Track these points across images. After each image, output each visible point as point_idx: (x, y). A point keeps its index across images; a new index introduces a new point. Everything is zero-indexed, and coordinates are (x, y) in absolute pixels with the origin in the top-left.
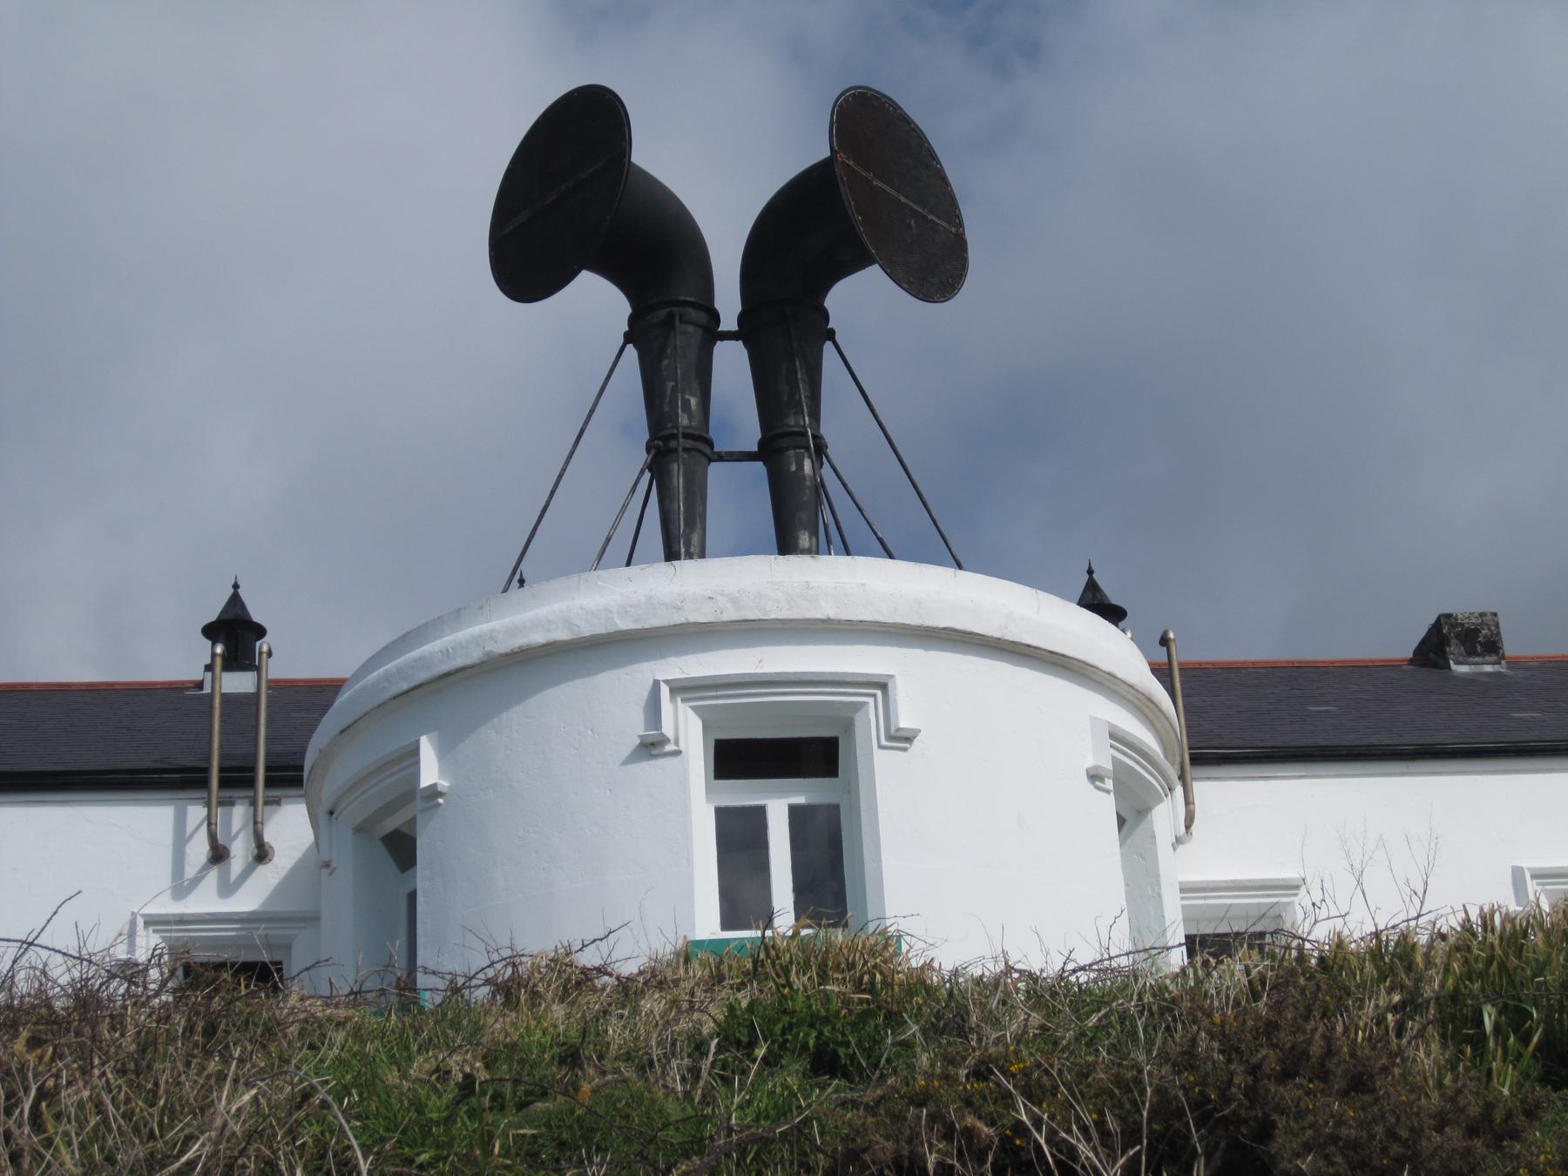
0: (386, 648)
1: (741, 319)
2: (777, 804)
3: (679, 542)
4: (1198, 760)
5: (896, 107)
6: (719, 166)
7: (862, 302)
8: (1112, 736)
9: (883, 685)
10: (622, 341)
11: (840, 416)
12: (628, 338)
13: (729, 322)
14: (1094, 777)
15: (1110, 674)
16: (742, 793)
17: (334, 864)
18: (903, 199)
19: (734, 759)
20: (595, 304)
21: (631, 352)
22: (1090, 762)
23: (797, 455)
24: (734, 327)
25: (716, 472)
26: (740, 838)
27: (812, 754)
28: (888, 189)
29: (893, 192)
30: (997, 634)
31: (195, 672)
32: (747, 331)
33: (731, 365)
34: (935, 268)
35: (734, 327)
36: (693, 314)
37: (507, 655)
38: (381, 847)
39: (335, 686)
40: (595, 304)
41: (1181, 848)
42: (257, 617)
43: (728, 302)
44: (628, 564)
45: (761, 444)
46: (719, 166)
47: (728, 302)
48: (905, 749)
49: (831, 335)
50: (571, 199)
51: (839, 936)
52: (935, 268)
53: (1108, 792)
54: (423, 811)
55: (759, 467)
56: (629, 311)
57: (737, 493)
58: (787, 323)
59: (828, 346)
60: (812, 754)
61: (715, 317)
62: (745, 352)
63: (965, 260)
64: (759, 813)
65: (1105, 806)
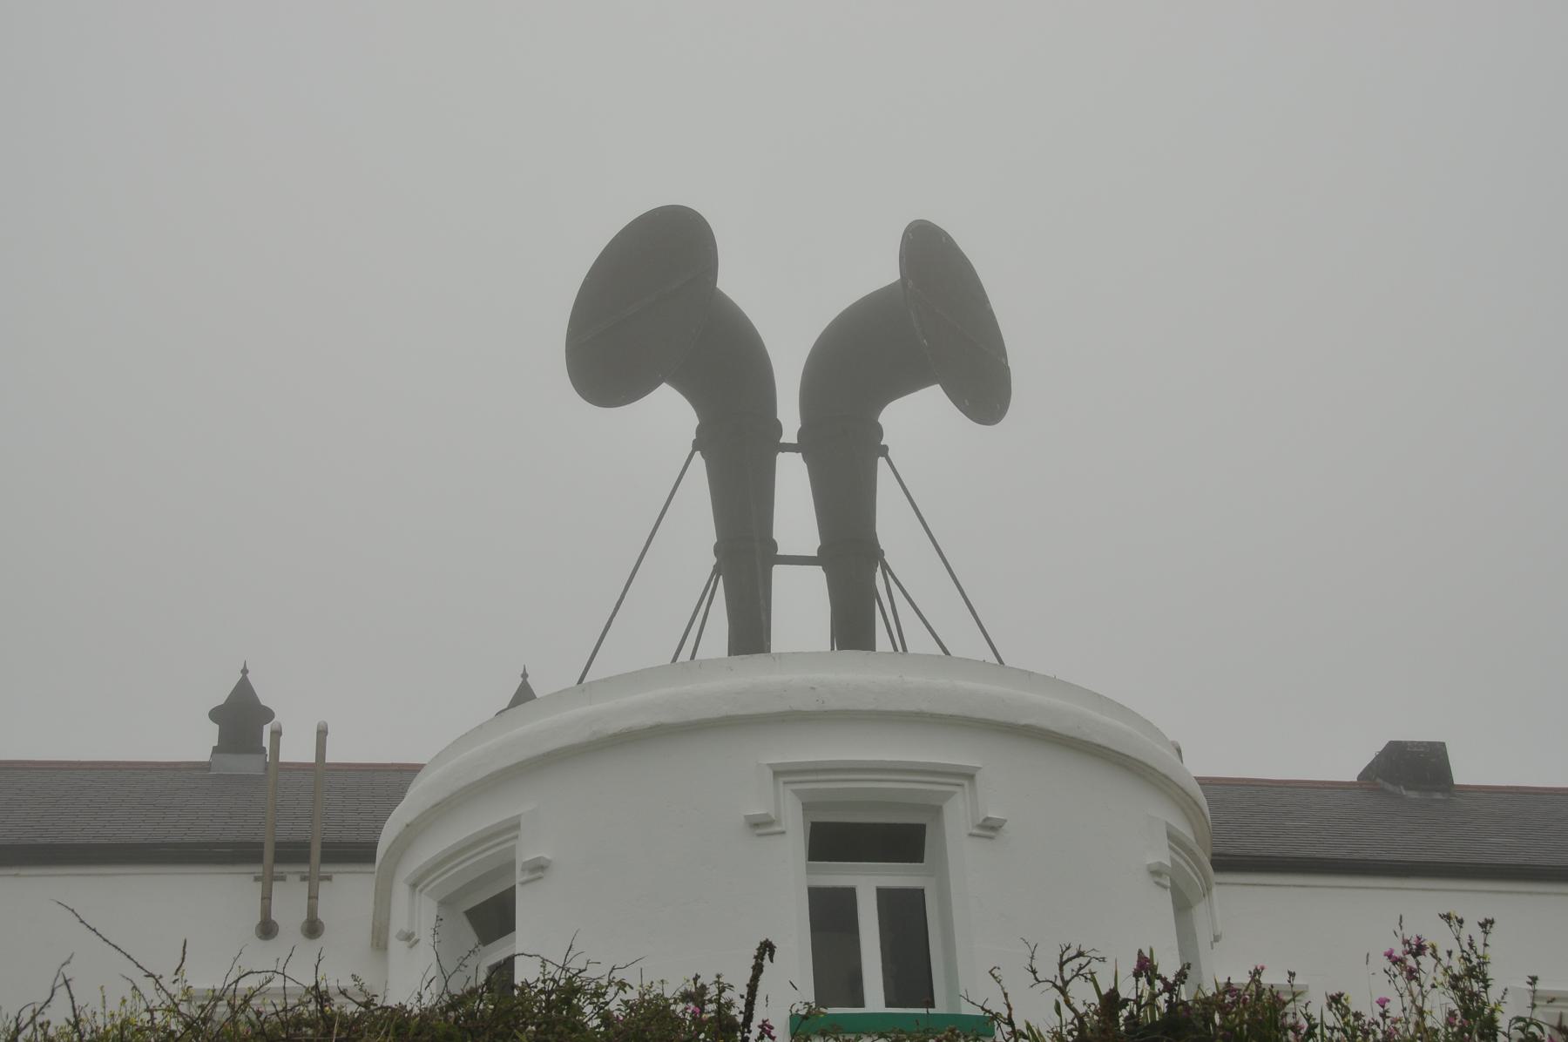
0: (481, 726)
1: (801, 434)
2: (868, 882)
4: (1226, 864)
5: (948, 238)
7: (917, 421)
8: (1170, 836)
9: (969, 776)
13: (790, 434)
14: (1156, 872)
16: (837, 875)
19: (830, 841)
20: (668, 415)
21: (699, 461)
22: (1152, 859)
26: (831, 915)
27: (904, 842)
31: (202, 754)
34: (983, 389)
37: (615, 735)
38: (465, 919)
39: (415, 769)
40: (668, 415)
41: (1444, 923)
42: (265, 699)
43: (790, 417)
47: (790, 417)
48: (991, 838)
49: (884, 451)
51: (931, 1011)
52: (983, 389)
53: (1165, 887)
54: (523, 883)
56: (697, 422)
57: (801, 602)
59: (882, 461)
61: (778, 428)
64: (847, 897)
65: (1165, 900)
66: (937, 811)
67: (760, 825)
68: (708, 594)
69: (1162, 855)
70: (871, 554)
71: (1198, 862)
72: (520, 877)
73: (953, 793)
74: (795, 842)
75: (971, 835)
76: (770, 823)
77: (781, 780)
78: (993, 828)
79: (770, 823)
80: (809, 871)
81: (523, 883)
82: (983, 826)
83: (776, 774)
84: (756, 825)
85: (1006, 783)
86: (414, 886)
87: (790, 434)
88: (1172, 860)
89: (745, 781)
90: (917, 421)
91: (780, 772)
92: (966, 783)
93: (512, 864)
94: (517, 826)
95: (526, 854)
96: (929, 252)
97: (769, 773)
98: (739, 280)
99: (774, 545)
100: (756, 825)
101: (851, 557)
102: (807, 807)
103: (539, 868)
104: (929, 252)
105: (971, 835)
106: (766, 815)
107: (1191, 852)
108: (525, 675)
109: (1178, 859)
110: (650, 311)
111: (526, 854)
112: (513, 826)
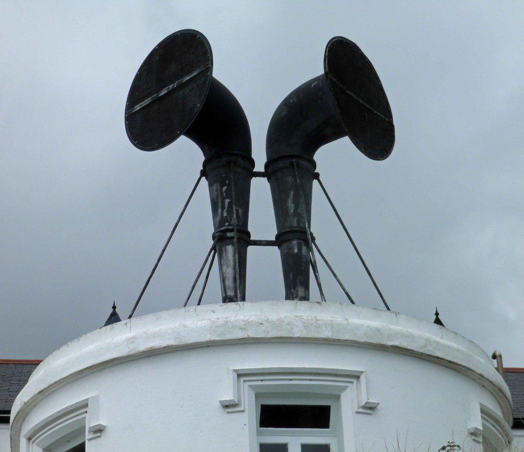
3: (235, 293)
6: (259, 80)
7: (337, 157)
9: (356, 376)
10: (199, 175)
11: (320, 222)
12: (203, 173)
13: (259, 167)
14: (474, 433)
15: (481, 375)
16: (276, 436)
17: (498, 354)
18: (361, 101)
20: (185, 154)
23: (298, 244)
24: (263, 170)
25: (251, 249)
28: (354, 96)
29: (356, 97)
30: (421, 351)
32: (270, 172)
33: (260, 191)
34: (377, 137)
35: (263, 170)
36: (240, 160)
43: (259, 155)
44: (199, 304)
45: (278, 237)
46: (259, 80)
47: (259, 155)
49: (317, 176)
50: (175, 92)
52: (377, 137)
53: (479, 443)
54: (90, 440)
55: (275, 251)
56: (203, 158)
57: (265, 263)
58: (293, 168)
59: (315, 182)
60: (318, 417)
61: (252, 163)
62: (268, 184)
63: (394, 136)
66: (338, 398)
67: (228, 406)
68: (207, 265)
69: (477, 423)
70: (305, 238)
71: (502, 427)
72: (88, 436)
73: (346, 388)
74: (249, 416)
75: (357, 412)
76: (235, 405)
77: (242, 379)
78: (371, 408)
79: (235, 405)
80: (258, 434)
81: (90, 440)
82: (364, 407)
83: (239, 376)
84: (227, 407)
85: (382, 380)
86: (29, 439)
87: (259, 167)
88: (484, 425)
89: (218, 379)
90: (337, 157)
91: (240, 375)
92: (355, 381)
93: (83, 428)
94: (86, 406)
95: (90, 423)
96: (345, 58)
97: (232, 377)
98: (225, 71)
99: (248, 234)
100: (227, 407)
101: (294, 239)
102: (258, 396)
103: (99, 431)
104: (345, 58)
105: (357, 412)
106: (232, 400)
107: (497, 421)
108: (114, 307)
109: (488, 425)
110: (175, 92)
111: (90, 423)
112: (84, 405)
